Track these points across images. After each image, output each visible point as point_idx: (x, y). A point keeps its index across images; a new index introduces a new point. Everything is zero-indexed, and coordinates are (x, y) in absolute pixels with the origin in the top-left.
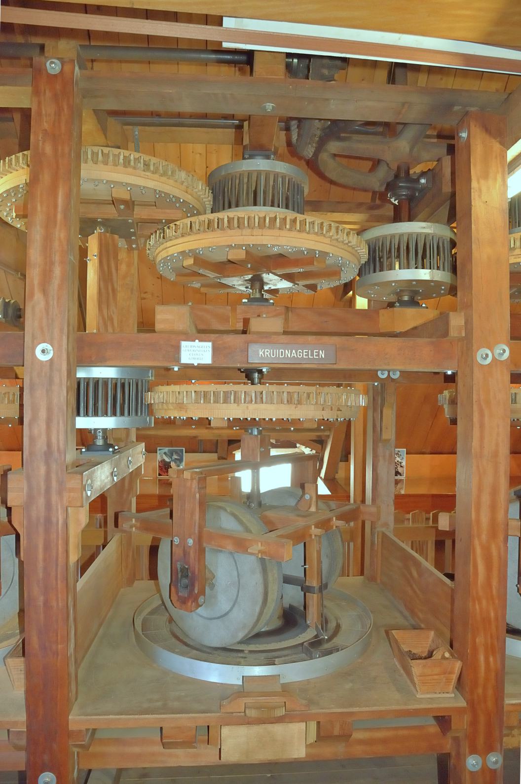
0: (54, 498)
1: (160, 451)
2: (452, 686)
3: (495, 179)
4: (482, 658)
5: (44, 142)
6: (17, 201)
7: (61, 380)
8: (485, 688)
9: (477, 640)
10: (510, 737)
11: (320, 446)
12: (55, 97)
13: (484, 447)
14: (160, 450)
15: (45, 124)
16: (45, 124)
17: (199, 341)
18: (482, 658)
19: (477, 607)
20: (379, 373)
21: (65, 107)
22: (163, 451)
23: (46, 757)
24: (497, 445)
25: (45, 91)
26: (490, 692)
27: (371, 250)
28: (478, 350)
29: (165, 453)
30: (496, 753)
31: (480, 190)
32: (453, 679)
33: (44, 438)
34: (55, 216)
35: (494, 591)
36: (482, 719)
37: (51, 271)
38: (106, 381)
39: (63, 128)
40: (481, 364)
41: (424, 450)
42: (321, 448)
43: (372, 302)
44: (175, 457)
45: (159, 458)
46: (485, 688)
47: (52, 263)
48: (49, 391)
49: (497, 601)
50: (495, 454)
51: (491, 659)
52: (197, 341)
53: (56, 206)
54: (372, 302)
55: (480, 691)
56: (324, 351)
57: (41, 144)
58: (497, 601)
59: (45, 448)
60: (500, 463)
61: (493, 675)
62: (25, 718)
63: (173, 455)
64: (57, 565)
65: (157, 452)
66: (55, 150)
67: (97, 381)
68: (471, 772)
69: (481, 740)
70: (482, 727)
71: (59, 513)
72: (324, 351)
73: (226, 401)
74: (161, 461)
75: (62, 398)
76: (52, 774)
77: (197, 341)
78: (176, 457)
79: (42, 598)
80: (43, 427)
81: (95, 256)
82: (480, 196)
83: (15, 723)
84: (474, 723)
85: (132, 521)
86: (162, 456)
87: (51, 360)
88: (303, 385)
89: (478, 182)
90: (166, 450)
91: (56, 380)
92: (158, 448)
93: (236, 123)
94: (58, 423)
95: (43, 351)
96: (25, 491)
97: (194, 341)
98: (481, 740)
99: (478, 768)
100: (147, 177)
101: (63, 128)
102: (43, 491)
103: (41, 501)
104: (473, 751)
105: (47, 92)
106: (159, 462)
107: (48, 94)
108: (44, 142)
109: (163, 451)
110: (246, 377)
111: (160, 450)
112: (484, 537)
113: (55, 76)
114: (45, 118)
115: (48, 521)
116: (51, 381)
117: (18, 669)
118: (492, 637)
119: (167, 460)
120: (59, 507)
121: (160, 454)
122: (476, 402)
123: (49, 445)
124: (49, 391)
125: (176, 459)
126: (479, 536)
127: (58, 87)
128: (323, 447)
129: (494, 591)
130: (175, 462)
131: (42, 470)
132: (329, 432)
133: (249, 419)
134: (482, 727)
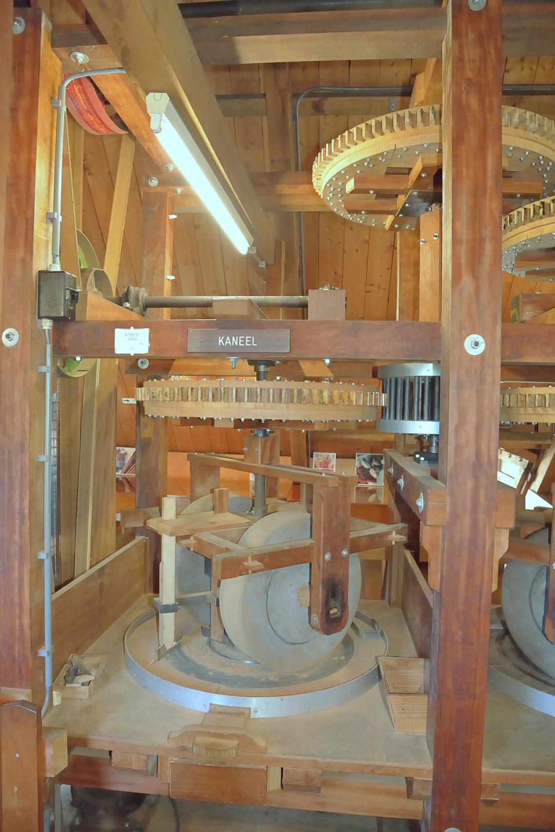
0: (481, 518)
1: (359, 457)
5: (468, 93)
6: (375, 167)
7: (494, 379)
11: (536, 456)
12: (480, 39)
14: (358, 455)
15: (468, 72)
16: (468, 72)
17: (135, 328)
21: (493, 51)
22: (362, 457)
23: (453, 812)
25: (467, 31)
27: (22, 239)
29: (364, 460)
33: (472, 447)
34: (484, 181)
37: (481, 248)
39: (490, 75)
42: (536, 458)
44: (375, 463)
45: (357, 464)
47: (482, 240)
48: (480, 392)
52: (132, 328)
53: (485, 171)
56: (220, 344)
57: (464, 96)
59: (473, 458)
62: (432, 767)
63: (372, 462)
64: (481, 595)
65: (355, 458)
66: (482, 102)
71: (487, 534)
72: (220, 344)
73: (205, 398)
74: (359, 468)
75: (495, 401)
76: (454, 829)
77: (132, 328)
78: (376, 464)
79: (460, 633)
80: (472, 433)
81: (436, 236)
83: (420, 772)
86: (360, 463)
87: (482, 355)
90: (365, 455)
91: (489, 379)
92: (357, 454)
93: (399, 90)
94: (490, 430)
95: (477, 344)
96: (448, 509)
97: (129, 328)
100: (536, 140)
101: (490, 75)
102: (468, 509)
103: (467, 520)
105: (469, 33)
106: (357, 469)
107: (471, 36)
108: (468, 93)
109: (362, 457)
111: (358, 455)
113: (479, 13)
114: (468, 65)
115: (473, 543)
116: (482, 381)
117: (400, 707)
119: (366, 466)
120: (487, 528)
121: (358, 460)
123: (478, 455)
124: (480, 392)
125: (375, 466)
127: (483, 26)
128: (540, 457)
130: (375, 469)
131: (470, 484)
132: (550, 440)
133: (243, 420)
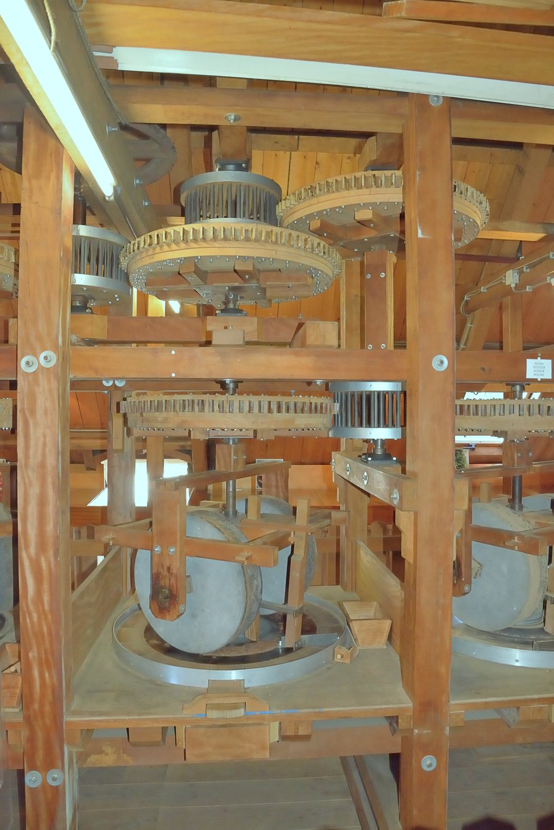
2: (16, 701)
3: (49, 178)
4: (36, 673)
8: (41, 704)
9: (30, 655)
10: (104, 755)
13: (30, 458)
18: (36, 673)
19: (28, 621)
20: (104, 383)
24: (44, 455)
26: (47, 708)
28: (22, 358)
30: (57, 770)
31: (31, 191)
32: (17, 694)
35: (46, 607)
36: (40, 735)
38: (385, 393)
40: (26, 373)
41: (303, 460)
42: (190, 458)
43: (201, 308)
46: (41, 704)
49: (50, 617)
50: (42, 465)
51: (47, 675)
54: (201, 308)
55: (36, 706)
58: (50, 617)
60: (48, 474)
61: (49, 691)
67: (369, 396)
68: (31, 789)
69: (40, 756)
70: (40, 743)
82: (30, 197)
84: (32, 739)
85: (514, 539)
88: (219, 393)
89: (30, 181)
95: (28, 363)
98: (40, 756)
99: (38, 784)
104: (33, 767)
110: (221, 388)
112: (32, 550)
118: (46, 651)
122: (20, 411)
126: (27, 547)
129: (46, 607)
134: (40, 743)
